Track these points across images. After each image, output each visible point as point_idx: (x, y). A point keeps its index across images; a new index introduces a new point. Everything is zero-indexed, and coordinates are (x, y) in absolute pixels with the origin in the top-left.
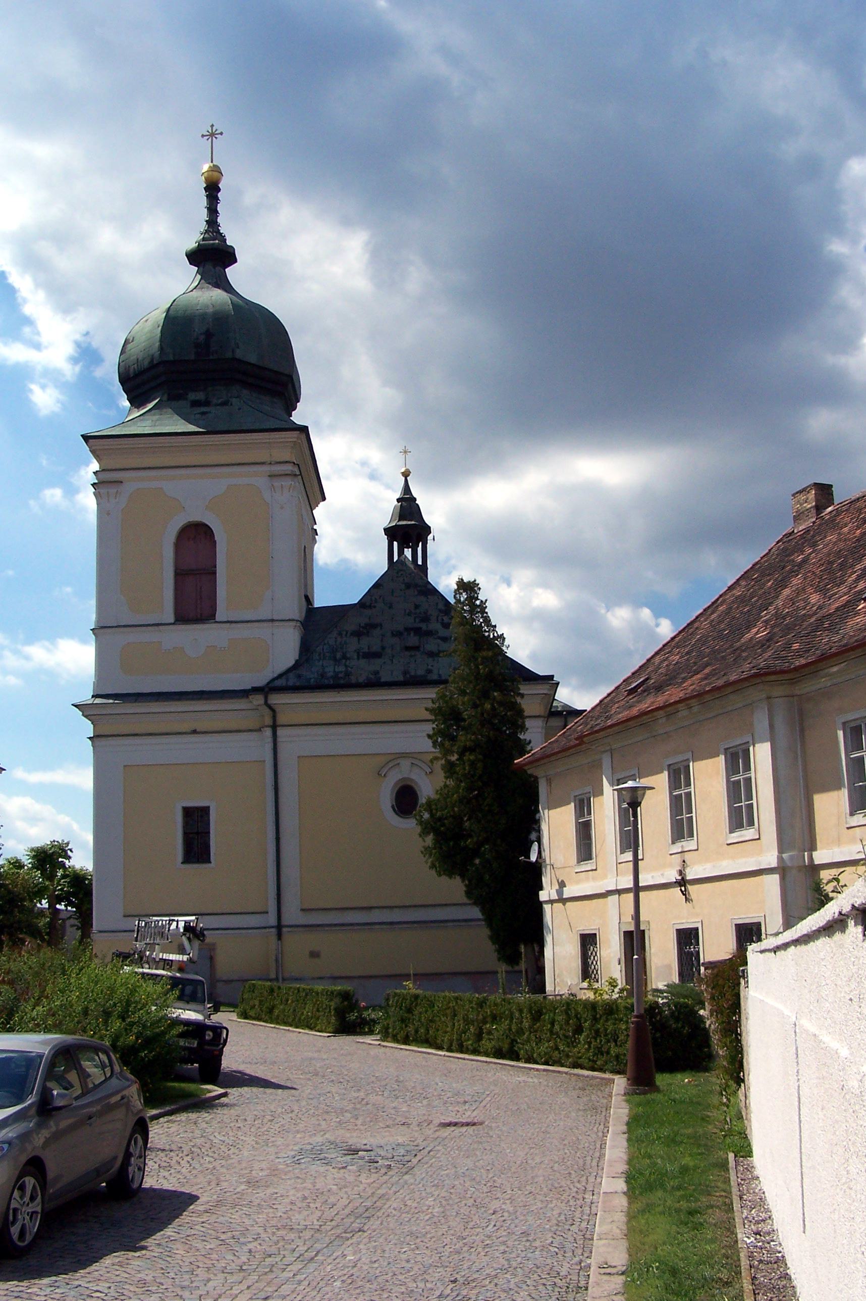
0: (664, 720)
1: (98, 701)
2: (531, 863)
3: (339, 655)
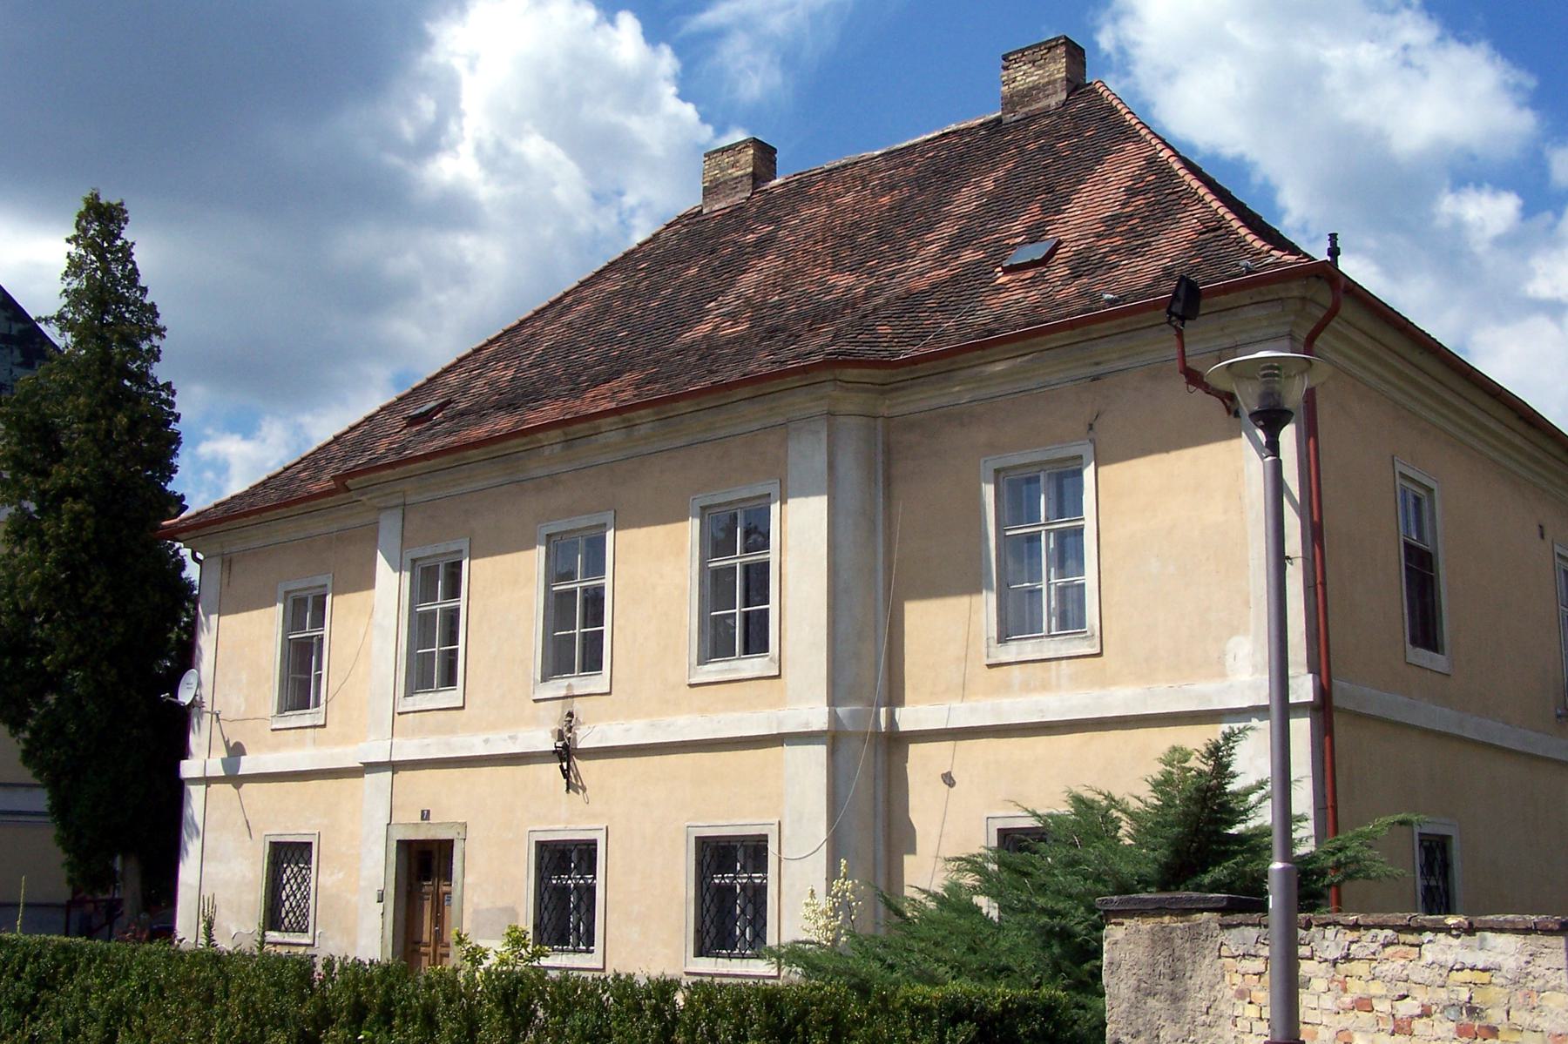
0: (558, 448)
2: (178, 706)
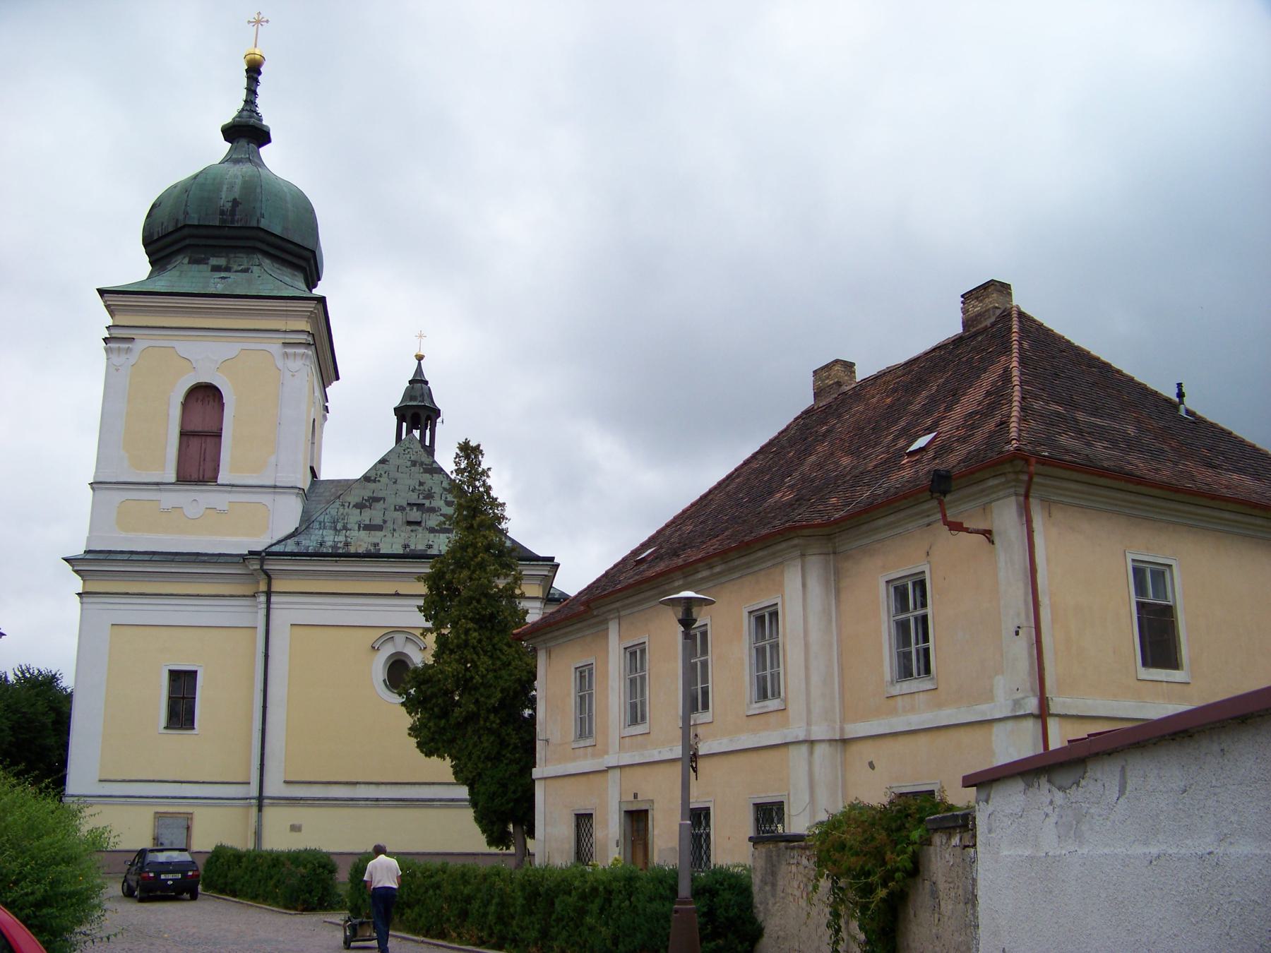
1: (88, 556)
3: (339, 526)
